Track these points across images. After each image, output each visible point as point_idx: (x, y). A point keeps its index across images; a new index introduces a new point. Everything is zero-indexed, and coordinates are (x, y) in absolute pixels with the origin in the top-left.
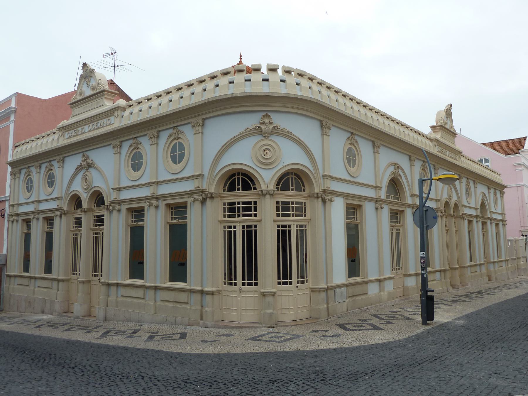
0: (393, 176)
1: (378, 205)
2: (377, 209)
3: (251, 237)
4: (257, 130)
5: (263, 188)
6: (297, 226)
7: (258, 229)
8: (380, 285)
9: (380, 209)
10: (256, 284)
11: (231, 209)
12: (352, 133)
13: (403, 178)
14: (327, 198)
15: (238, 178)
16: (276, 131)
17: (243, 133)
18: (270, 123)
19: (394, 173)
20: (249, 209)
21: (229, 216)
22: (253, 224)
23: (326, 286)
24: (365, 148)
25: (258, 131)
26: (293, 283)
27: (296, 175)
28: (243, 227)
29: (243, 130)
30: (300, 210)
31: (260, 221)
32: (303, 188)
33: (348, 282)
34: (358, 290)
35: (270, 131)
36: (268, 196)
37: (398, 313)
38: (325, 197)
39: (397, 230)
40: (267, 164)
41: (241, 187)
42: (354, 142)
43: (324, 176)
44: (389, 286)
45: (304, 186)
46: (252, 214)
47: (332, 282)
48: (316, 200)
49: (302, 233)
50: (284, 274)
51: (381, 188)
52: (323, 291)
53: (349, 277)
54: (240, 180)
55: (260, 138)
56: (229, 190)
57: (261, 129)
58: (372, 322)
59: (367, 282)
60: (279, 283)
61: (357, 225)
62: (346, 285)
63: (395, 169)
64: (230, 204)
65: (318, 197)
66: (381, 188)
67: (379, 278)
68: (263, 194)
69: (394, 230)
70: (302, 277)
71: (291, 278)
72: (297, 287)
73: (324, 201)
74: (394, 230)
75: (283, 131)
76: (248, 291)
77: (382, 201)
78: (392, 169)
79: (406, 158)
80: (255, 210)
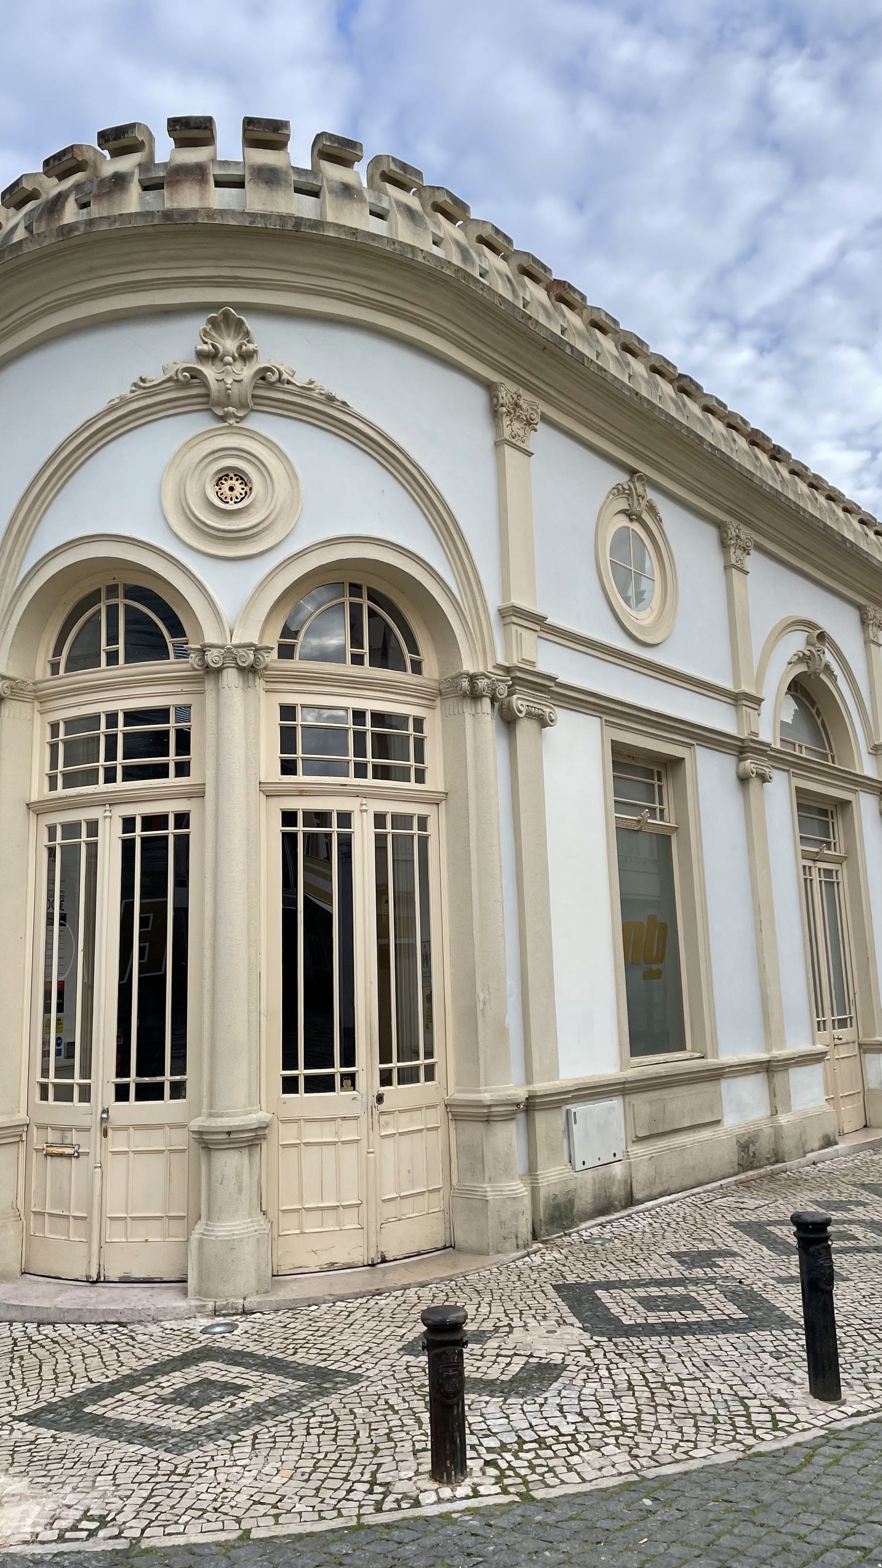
0: (802, 668)
1: (749, 765)
2: (743, 780)
3: (159, 864)
4: (185, 385)
5: (211, 637)
6: (379, 819)
7: (193, 830)
8: (770, 1082)
9: (755, 783)
10: (178, 1091)
11: (77, 752)
12: (633, 472)
13: (842, 682)
14: (519, 702)
15: (112, 611)
16: (271, 392)
17: (124, 401)
18: (246, 357)
19: (803, 659)
20: (155, 744)
21: (71, 780)
22: (170, 808)
23: (521, 1094)
24: (688, 541)
25: (189, 391)
26: (360, 1080)
27: (373, 596)
28: (128, 824)
29: (125, 390)
30: (387, 746)
31: (198, 794)
32: (408, 656)
33: (631, 1073)
34: (682, 1103)
35: (247, 389)
36: (231, 677)
37: (859, 1212)
38: (517, 701)
39: (828, 872)
40: (229, 539)
41: (121, 646)
42: (640, 507)
43: (512, 614)
44: (808, 1092)
45: (414, 648)
46: (166, 766)
47: (553, 1071)
48: (468, 708)
49: (403, 852)
50: (314, 1040)
51: (758, 701)
52: (509, 1117)
53: (633, 1054)
54: (132, 612)
55: (201, 423)
56: (74, 664)
57: (205, 384)
58: (738, 1268)
59: (716, 1074)
60: (290, 1085)
61: (663, 841)
62: (622, 1089)
63: (809, 643)
64: (72, 724)
65: (475, 696)
66: (758, 701)
67: (764, 1056)
68: (207, 669)
69: (815, 872)
70: (407, 1050)
71: (349, 1058)
72: (380, 1099)
73: (508, 721)
74: (815, 872)
75: (306, 390)
76: (138, 1127)
77: (762, 753)
78: (797, 642)
79: (851, 616)
80: (184, 745)
